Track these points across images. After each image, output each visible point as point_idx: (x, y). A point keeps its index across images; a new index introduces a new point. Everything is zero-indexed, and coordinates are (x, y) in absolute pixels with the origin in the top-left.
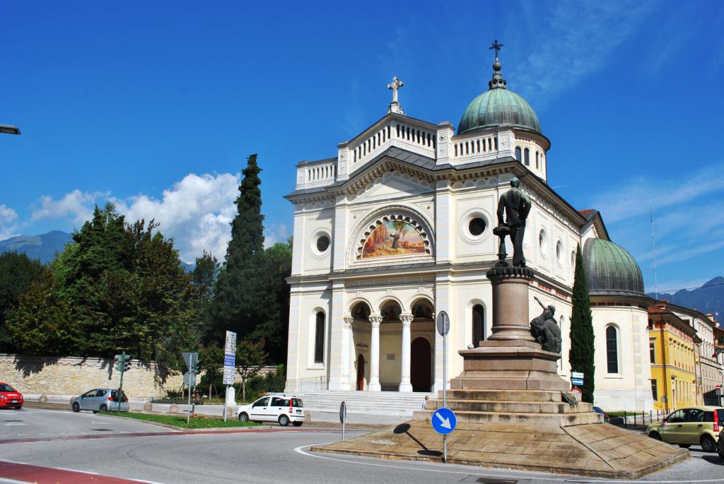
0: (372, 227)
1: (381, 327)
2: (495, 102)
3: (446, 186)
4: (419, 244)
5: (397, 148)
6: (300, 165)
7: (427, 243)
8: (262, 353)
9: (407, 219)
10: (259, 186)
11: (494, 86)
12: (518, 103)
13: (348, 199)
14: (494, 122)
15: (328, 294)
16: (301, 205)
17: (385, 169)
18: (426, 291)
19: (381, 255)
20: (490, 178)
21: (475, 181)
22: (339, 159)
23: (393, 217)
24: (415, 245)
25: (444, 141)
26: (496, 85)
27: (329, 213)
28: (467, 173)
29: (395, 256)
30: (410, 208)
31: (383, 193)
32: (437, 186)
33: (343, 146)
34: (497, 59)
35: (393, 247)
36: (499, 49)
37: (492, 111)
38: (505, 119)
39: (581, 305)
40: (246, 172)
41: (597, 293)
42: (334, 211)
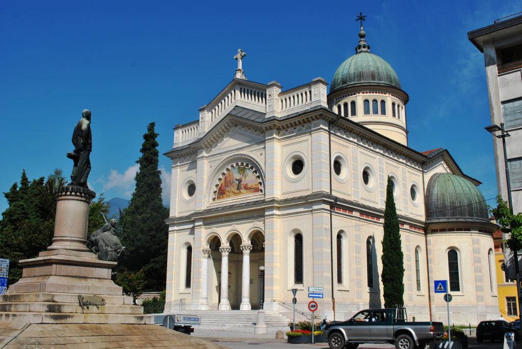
0: (223, 174)
1: (229, 257)
2: (355, 65)
3: (273, 135)
4: (256, 185)
6: (176, 128)
7: (260, 183)
8: (142, 281)
9: (247, 165)
10: (157, 148)
11: (359, 51)
12: (375, 62)
14: (354, 81)
15: (192, 231)
16: (176, 160)
18: (258, 224)
19: (229, 196)
20: (306, 125)
21: (295, 128)
22: (200, 121)
23: (237, 164)
24: (253, 186)
25: (272, 98)
26: (360, 50)
27: (193, 166)
28: (288, 122)
29: (239, 197)
30: (248, 156)
31: (231, 144)
32: (266, 135)
33: (202, 110)
34: (362, 28)
35: (238, 189)
36: (364, 20)
37: (352, 72)
38: (363, 77)
39: (390, 230)
40: (146, 137)
41: (438, 221)
42: (196, 164)
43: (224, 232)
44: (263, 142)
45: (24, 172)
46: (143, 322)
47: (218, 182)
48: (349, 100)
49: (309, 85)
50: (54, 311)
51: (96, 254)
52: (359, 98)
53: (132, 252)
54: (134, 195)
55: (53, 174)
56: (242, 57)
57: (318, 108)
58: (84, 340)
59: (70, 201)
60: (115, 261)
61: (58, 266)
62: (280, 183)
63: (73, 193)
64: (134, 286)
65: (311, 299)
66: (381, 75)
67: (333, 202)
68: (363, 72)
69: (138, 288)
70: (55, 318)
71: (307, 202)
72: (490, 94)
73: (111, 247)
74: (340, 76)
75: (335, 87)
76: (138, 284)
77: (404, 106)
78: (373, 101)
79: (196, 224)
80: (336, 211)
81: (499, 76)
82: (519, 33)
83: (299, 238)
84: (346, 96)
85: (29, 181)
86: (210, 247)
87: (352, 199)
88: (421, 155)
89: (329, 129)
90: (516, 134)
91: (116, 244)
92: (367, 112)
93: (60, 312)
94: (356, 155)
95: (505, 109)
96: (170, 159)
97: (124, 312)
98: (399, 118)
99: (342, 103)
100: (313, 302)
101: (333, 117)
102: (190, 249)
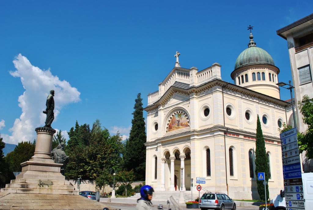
0: (171, 118)
1: (175, 162)
2: (247, 54)
3: (193, 96)
5: (177, 82)
6: (149, 95)
9: (182, 113)
12: (258, 52)
13: (162, 107)
14: (246, 63)
17: (173, 92)
19: (174, 130)
22: (159, 91)
23: (177, 112)
26: (250, 46)
27: (156, 115)
29: (179, 130)
31: (173, 102)
33: (160, 85)
34: (251, 34)
35: (178, 126)
37: (245, 58)
38: (251, 60)
40: (136, 101)
43: (171, 149)
44: (189, 100)
45: (77, 121)
46: (73, 194)
47: (168, 123)
48: (244, 74)
49: (210, 67)
50: (24, 188)
51: (54, 160)
52: (250, 72)
53: (130, 161)
54: (131, 131)
55: (95, 122)
56: (178, 56)
57: (215, 79)
58: (33, 201)
59: (41, 134)
60: (62, 163)
61: (31, 166)
62: (198, 122)
63: (43, 131)
64: (128, 178)
65: (198, 184)
66: (261, 58)
67: (225, 131)
68: (251, 58)
69: (130, 179)
70: (23, 190)
71: (211, 131)
72: (291, 64)
73: (60, 157)
74: (239, 61)
75: (236, 67)
76: (131, 177)
77: (277, 75)
78: (257, 73)
79: (158, 145)
80: (228, 135)
81: (296, 54)
82: (311, 26)
83: (208, 151)
84: (242, 72)
85: (79, 126)
86: (166, 157)
87: (238, 128)
88: (284, 101)
89: (222, 90)
90: (306, 86)
91: (63, 155)
92: (254, 79)
93: (27, 188)
94: (240, 104)
95: (300, 72)
96: (146, 111)
97: (63, 189)
98: (273, 81)
99: (240, 76)
100: (199, 185)
101: (224, 84)
102: (156, 158)
